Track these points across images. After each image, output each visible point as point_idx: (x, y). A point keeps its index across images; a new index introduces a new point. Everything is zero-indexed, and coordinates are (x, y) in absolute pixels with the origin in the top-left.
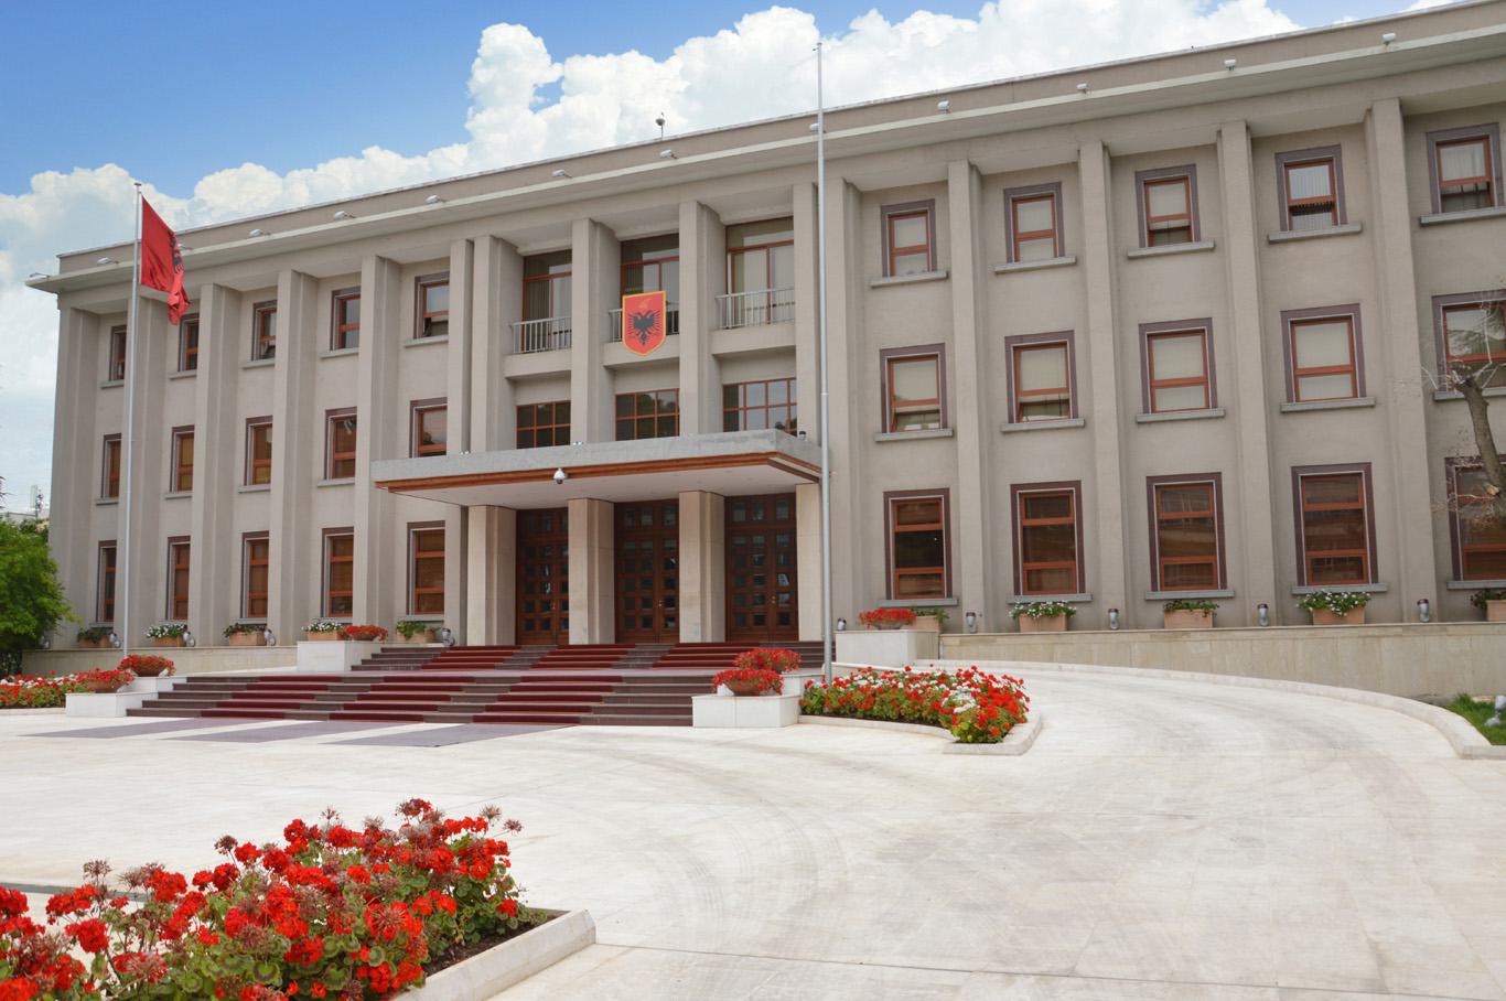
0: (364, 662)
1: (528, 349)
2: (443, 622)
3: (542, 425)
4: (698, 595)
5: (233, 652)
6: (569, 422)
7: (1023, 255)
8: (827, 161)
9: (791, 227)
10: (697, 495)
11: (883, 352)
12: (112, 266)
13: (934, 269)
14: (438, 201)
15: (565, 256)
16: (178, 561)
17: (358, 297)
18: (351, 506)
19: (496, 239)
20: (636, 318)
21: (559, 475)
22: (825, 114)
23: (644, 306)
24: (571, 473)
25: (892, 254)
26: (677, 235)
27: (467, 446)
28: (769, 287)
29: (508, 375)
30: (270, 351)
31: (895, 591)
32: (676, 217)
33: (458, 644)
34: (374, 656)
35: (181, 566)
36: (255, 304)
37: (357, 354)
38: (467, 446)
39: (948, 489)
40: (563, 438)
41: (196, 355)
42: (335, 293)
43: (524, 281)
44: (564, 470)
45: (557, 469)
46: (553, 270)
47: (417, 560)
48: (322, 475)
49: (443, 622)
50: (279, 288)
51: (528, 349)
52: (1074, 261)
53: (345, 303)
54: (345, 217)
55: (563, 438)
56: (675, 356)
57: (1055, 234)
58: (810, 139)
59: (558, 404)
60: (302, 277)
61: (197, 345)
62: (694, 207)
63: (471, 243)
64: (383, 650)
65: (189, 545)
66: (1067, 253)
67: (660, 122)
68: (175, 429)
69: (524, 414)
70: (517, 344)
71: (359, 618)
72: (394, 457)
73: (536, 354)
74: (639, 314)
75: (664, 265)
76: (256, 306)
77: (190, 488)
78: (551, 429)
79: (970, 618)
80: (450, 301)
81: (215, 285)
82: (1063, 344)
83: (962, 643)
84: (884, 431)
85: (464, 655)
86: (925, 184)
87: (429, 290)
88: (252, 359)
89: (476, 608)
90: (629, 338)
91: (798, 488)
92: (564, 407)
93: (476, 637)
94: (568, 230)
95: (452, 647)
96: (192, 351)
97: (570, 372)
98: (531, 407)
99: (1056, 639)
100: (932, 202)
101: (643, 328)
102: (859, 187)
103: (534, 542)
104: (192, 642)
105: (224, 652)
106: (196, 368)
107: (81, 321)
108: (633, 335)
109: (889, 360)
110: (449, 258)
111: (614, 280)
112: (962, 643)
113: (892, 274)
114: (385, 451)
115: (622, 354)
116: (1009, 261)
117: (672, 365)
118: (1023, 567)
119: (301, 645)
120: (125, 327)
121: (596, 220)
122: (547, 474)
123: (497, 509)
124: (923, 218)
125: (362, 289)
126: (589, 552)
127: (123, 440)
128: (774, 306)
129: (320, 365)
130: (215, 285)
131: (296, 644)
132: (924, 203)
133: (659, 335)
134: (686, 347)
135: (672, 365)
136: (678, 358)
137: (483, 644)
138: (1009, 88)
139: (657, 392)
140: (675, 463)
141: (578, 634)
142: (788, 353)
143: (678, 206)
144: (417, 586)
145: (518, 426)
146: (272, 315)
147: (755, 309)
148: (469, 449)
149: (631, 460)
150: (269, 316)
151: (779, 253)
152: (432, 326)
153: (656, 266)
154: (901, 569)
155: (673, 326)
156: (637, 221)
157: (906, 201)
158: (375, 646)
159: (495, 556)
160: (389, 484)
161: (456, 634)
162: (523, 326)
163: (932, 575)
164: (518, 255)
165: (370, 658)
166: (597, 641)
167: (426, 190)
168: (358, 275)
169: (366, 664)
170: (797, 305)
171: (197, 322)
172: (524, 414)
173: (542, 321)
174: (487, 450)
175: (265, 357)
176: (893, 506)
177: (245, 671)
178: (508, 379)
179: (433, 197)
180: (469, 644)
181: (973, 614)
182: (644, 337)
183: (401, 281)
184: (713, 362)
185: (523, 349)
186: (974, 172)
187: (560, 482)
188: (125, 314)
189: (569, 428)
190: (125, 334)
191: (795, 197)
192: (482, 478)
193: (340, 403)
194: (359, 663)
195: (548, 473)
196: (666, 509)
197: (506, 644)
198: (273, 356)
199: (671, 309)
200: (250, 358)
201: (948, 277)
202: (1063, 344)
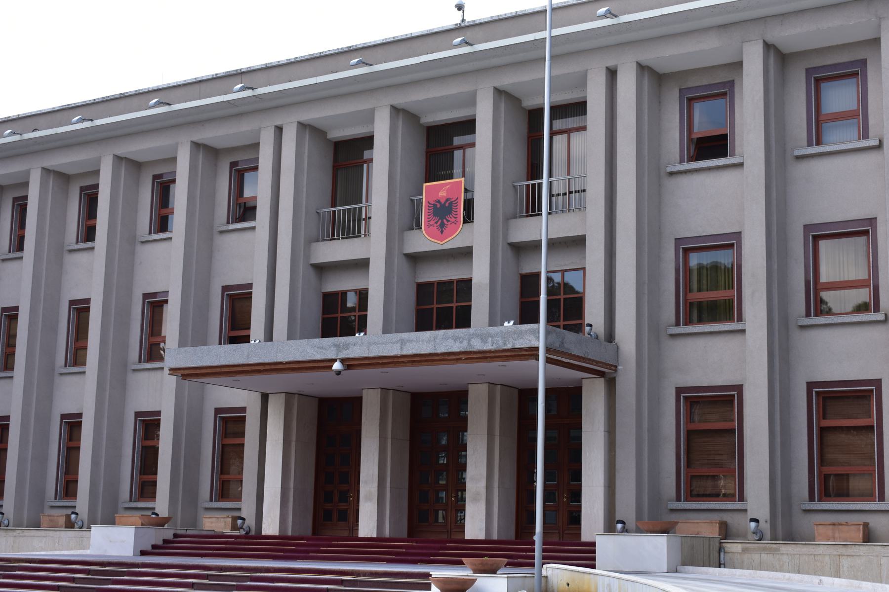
0: (154, 547)
1: (348, 233)
2: (239, 509)
3: (339, 316)
5: (43, 533)
7: (825, 137)
8: (552, 57)
9: (473, 131)
10: (485, 387)
11: (678, 241)
13: (866, 136)
14: (14, 133)
15: (468, 126)
16: (70, 439)
17: (256, 168)
18: (157, 392)
20: (435, 205)
21: (337, 366)
22: (554, 10)
23: (443, 194)
24: (350, 364)
25: (819, 124)
26: (585, 102)
27: (269, 336)
28: (569, 174)
30: (20, 247)
32: (371, 120)
33: (253, 533)
34: (165, 541)
35: (72, 444)
36: (231, 163)
38: (269, 336)
40: (463, 319)
41: (95, 227)
42: (155, 177)
44: (342, 361)
45: (335, 360)
46: (457, 141)
47: (223, 446)
48: (673, 319)
49: (75, 507)
51: (348, 233)
52: (877, 143)
53: (243, 175)
54: (159, 104)
55: (463, 319)
56: (467, 244)
58: (557, 32)
59: (459, 282)
61: (95, 218)
62: (39, 171)
63: (279, 130)
64: (175, 535)
65: (245, 417)
66: (871, 134)
67: (460, 7)
68: (225, 288)
69: (423, 290)
71: (162, 505)
72: (205, 343)
73: (341, 241)
74: (439, 201)
76: (82, 189)
77: (12, 369)
79: (753, 524)
80: (259, 188)
81: (392, 106)
82: (866, 233)
83: (744, 550)
85: (252, 543)
86: (725, 65)
87: (823, 85)
89: (270, 499)
90: (428, 226)
92: (466, 285)
93: (271, 527)
94: (472, 100)
95: (247, 535)
97: (369, 259)
98: (430, 284)
99: (842, 550)
100: (863, 63)
103: (329, 429)
104: (6, 522)
105: (32, 533)
106: (93, 240)
108: (432, 222)
109: (814, 237)
110: (258, 144)
111: (418, 166)
112: (744, 550)
113: (819, 143)
114: (193, 336)
115: (422, 241)
116: (810, 144)
117: (466, 253)
119: (94, 528)
120: (26, 198)
121: (644, 63)
122: (325, 365)
123: (499, 387)
125: (261, 160)
129: (140, 248)
130: (392, 106)
131: (90, 528)
132: (723, 84)
133: (456, 223)
134: (374, 246)
135: (466, 253)
137: (482, 537)
138: (197, 86)
139: (563, 272)
140: (446, 357)
141: (367, 526)
142: (578, 242)
144: (222, 473)
145: (323, 313)
146: (172, 186)
151: (576, 138)
152: (244, 211)
153: (566, 136)
155: (469, 217)
156: (437, 104)
158: (167, 533)
159: (293, 444)
160: (182, 372)
161: (251, 522)
165: (160, 543)
166: (387, 533)
167: (71, 112)
168: (174, 160)
169: (156, 550)
170: (372, 220)
171: (97, 193)
172: (423, 290)
175: (242, 219)
178: (312, 265)
180: (263, 533)
181: (756, 521)
182: (442, 226)
183: (216, 165)
184: (509, 253)
185: (527, 211)
187: (338, 373)
188: (26, 185)
189: (366, 315)
190: (26, 205)
191: (589, 82)
193: (236, 279)
194: (149, 548)
195: (328, 364)
196: (457, 399)
198: (253, 218)
199: (469, 196)
200: (75, 240)
201: (880, 146)
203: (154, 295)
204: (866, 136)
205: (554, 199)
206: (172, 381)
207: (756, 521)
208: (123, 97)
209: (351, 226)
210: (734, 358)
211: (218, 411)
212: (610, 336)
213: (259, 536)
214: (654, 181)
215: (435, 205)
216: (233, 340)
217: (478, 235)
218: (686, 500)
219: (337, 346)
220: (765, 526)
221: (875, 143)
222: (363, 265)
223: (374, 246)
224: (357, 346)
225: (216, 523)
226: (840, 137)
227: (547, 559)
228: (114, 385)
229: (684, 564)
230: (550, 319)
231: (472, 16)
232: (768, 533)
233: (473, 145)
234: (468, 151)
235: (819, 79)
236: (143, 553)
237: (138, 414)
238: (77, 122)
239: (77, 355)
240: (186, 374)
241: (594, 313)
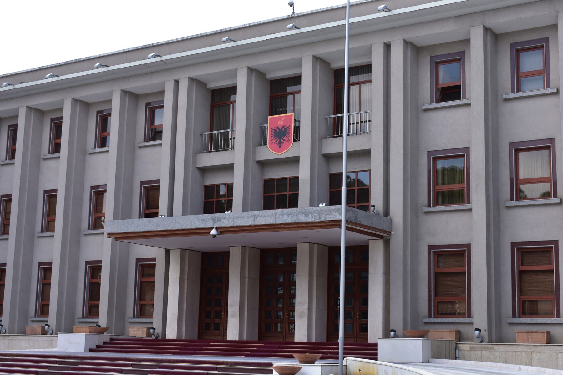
0: (98, 346)
3: (215, 200)
4: (306, 311)
6: (297, 190)
7: (522, 87)
9: (299, 83)
10: (308, 245)
11: (430, 153)
12: (157, 59)
13: (548, 86)
14: (9, 85)
15: (297, 80)
17: (162, 107)
18: (99, 248)
19: (191, 80)
20: (275, 130)
21: (213, 232)
22: (351, 6)
23: (280, 123)
24: (221, 231)
25: (518, 79)
27: (170, 213)
28: (360, 110)
29: (323, 153)
30: (13, 156)
31: (434, 312)
32: (235, 76)
33: (160, 338)
34: (105, 343)
35: (46, 281)
37: (59, 157)
38: (170, 213)
39: (557, 241)
40: (294, 203)
42: (98, 112)
43: (211, 105)
44: (217, 229)
46: (290, 89)
47: (142, 283)
49: (152, 323)
50: (165, 91)
54: (101, 66)
55: (294, 203)
56: (296, 155)
57: (544, 73)
59: (291, 178)
60: (254, 73)
63: (177, 82)
64: (111, 339)
67: (291, 5)
68: (142, 183)
69: (268, 184)
70: (330, 130)
71: (102, 320)
74: (278, 128)
75: (363, 86)
76: (52, 120)
78: (286, 195)
79: (477, 332)
80: (164, 119)
81: (73, 99)
82: (548, 148)
83: (471, 349)
84: (429, 205)
85: (160, 344)
86: (459, 41)
87: (521, 54)
88: (49, 154)
89: (171, 316)
90: (271, 143)
91: (370, 242)
92: (295, 181)
93: (171, 334)
94: (299, 63)
95: (157, 339)
96: (57, 141)
98: (273, 180)
99: (534, 349)
100: (547, 40)
101: (280, 134)
102: (416, 44)
103: (208, 272)
105: (20, 338)
106: (59, 152)
107: (127, 99)
108: (274, 141)
109: (516, 150)
111: (265, 105)
112: (471, 349)
113: (518, 91)
114: (122, 213)
115: (268, 153)
116: (513, 91)
117: (295, 161)
118: (519, 299)
119: (60, 335)
120: (16, 125)
121: (408, 40)
122: (206, 231)
123: (316, 245)
124: (541, 51)
126: (309, 279)
127: (161, 184)
128: (358, 123)
130: (73, 99)
132: (458, 53)
133: (289, 141)
134: (237, 156)
135: (295, 161)
136: (299, 156)
138: (125, 55)
139: (357, 172)
141: (233, 333)
142: (366, 154)
143: (301, 58)
145: (205, 199)
146: (109, 118)
147: (354, 124)
148: (172, 215)
149: (177, 227)
150: (107, 119)
151: (365, 87)
152: (155, 134)
154: (92, 302)
155: (297, 138)
156: (277, 66)
157: (447, 52)
158: (106, 338)
161: (159, 331)
162: (334, 118)
163: (448, 302)
164: (331, 69)
165: (102, 344)
167: (45, 71)
168: (110, 101)
171: (61, 123)
172: (268, 184)
173: (220, 131)
174: (114, 219)
175: (153, 139)
176: (518, 253)
177: (36, 350)
179: (5, 83)
180: (167, 338)
181: (479, 330)
182: (280, 143)
183: (137, 105)
184: (323, 160)
185: (334, 134)
186: (489, 33)
187: (214, 236)
188: (16, 117)
189: (232, 200)
190: (16, 130)
192: (169, 233)
193: (50, 187)
195: (208, 231)
196: (290, 253)
197: (251, 340)
198: (161, 138)
199: (297, 124)
200: (47, 152)
201: (557, 93)
202: (548, 148)
203: (98, 187)
204: (548, 86)
205: (351, 126)
206: (109, 241)
207: (479, 330)
208: (78, 62)
209: (222, 143)
210: (465, 227)
211: (138, 260)
212: (387, 213)
213: (164, 339)
214: (414, 114)
215: (275, 130)
216: (148, 216)
217: (303, 149)
218: (435, 317)
219: (213, 219)
220: (485, 333)
221: (555, 91)
222: (230, 168)
223: (237, 156)
224: (226, 219)
225: (137, 332)
226: (532, 87)
227: (347, 354)
228: (72, 244)
229: (433, 357)
230: (348, 202)
231: (299, 10)
232: (486, 338)
233: (299, 92)
234: (297, 96)
235: (518, 50)
236: (91, 350)
237: (87, 263)
238: (49, 77)
239: (49, 225)
240: (118, 237)
241: (376, 198)
